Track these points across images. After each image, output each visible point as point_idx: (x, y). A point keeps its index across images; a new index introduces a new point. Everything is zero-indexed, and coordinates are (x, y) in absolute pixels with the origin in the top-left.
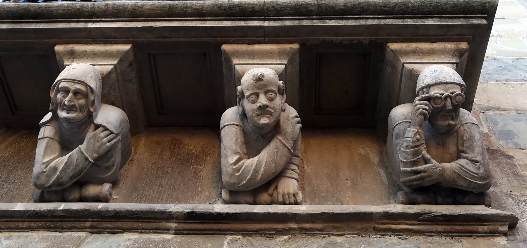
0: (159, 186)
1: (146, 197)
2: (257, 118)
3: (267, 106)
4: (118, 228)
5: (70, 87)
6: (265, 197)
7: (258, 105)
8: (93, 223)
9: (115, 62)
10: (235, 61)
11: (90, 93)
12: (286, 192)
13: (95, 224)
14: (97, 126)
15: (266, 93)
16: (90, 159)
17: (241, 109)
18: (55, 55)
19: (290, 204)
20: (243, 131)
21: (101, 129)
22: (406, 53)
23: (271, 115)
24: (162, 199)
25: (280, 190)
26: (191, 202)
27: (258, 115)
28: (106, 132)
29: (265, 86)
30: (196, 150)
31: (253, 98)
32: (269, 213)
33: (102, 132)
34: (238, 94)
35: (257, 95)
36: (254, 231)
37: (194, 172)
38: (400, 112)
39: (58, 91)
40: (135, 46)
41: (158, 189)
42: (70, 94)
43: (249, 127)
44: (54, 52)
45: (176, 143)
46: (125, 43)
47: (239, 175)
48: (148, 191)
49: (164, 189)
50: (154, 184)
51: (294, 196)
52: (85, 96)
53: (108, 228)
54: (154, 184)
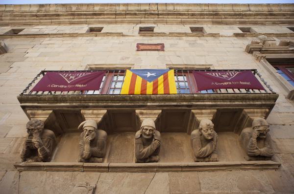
6: (207, 159)
10: (196, 116)
35: (207, 130)
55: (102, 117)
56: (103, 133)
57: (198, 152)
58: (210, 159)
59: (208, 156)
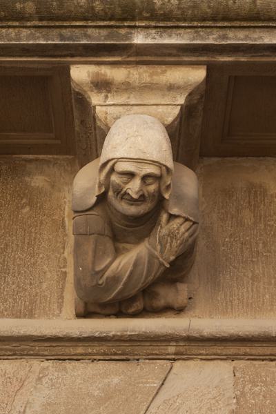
0: (252, 279)
8: (178, 348)
13: (182, 349)
14: (172, 217)
24: (263, 302)
28: (188, 224)
40: (211, 69)
41: (253, 284)
48: (239, 289)
52: (158, 178)
55: (181, 100)
56: (188, 182)
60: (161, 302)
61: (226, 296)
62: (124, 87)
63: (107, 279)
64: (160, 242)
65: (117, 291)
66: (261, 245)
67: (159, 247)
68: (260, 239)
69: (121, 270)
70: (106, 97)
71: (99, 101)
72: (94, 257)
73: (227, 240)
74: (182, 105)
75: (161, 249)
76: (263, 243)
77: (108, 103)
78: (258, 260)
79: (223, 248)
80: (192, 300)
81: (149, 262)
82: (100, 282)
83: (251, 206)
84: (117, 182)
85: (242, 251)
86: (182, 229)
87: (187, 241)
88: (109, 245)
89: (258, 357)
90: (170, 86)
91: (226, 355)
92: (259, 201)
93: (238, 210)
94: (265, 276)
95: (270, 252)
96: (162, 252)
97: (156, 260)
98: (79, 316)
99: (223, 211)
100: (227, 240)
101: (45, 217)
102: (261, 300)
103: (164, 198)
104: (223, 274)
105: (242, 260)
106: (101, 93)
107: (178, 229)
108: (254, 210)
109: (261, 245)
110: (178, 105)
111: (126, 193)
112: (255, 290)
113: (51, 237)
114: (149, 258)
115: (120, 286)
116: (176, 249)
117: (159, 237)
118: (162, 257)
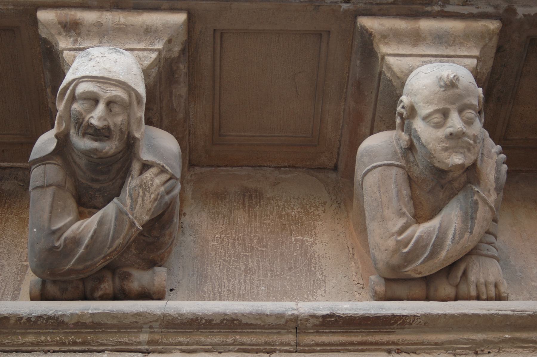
1: (229, 290)
2: (446, 154)
3: (464, 133)
4: (197, 344)
5: (101, 93)
7: (449, 130)
9: (159, 46)
10: (384, 49)
11: (135, 103)
12: (482, 280)
13: (157, 337)
14: (146, 166)
15: (461, 111)
16: (137, 224)
17: (405, 137)
18: (37, 27)
19: (489, 299)
20: (409, 176)
21: (153, 171)
22: (385, 37)
23: (469, 150)
24: (258, 293)
25: (472, 278)
26: (310, 297)
27: (446, 149)
29: (460, 97)
30: (293, 209)
31: (437, 118)
32: (465, 315)
33: (157, 175)
34: (399, 109)
35: (445, 114)
36: (436, 344)
37: (301, 247)
38: (377, 144)
39: (73, 98)
41: (245, 277)
42: (101, 107)
43: (418, 170)
44: (35, 21)
45: (251, 196)
46: (173, 9)
47: (408, 252)
48: (229, 281)
49: (256, 277)
50: (236, 268)
51: (496, 286)
53: (180, 344)
54: (236, 268)
57: (391, 243)
58: (463, 288)
59: (449, 270)
60: (135, 286)
61: (213, 287)
62: (95, 29)
63: (65, 240)
64: (130, 196)
65: (77, 256)
66: (255, 241)
67: (128, 202)
68: (255, 236)
69: (82, 230)
70: (76, 41)
71: (67, 45)
72: (51, 213)
73: (217, 236)
74: (159, 51)
75: (131, 204)
76: (259, 239)
77: (77, 46)
78: (252, 255)
79: (212, 243)
80: (173, 291)
81: (116, 218)
82: (57, 244)
83: (245, 207)
84: (78, 109)
85: (234, 246)
86: (157, 181)
87: (162, 197)
88: (72, 204)
89: (250, 347)
90: (147, 29)
91: (211, 344)
92: (254, 203)
93: (231, 211)
94: (260, 269)
95: (266, 247)
96: (132, 208)
97: (125, 217)
98: (32, 299)
99: (214, 211)
100: (217, 236)
101: (13, 215)
102: (256, 291)
103: (135, 139)
104: (211, 266)
105: (234, 254)
106: (70, 37)
107: (152, 179)
108: (249, 210)
109: (255, 241)
110: (156, 50)
111: (90, 126)
112: (248, 282)
113: (15, 233)
114: (116, 213)
115: (81, 250)
116: (150, 206)
117: (130, 190)
118: (133, 214)
